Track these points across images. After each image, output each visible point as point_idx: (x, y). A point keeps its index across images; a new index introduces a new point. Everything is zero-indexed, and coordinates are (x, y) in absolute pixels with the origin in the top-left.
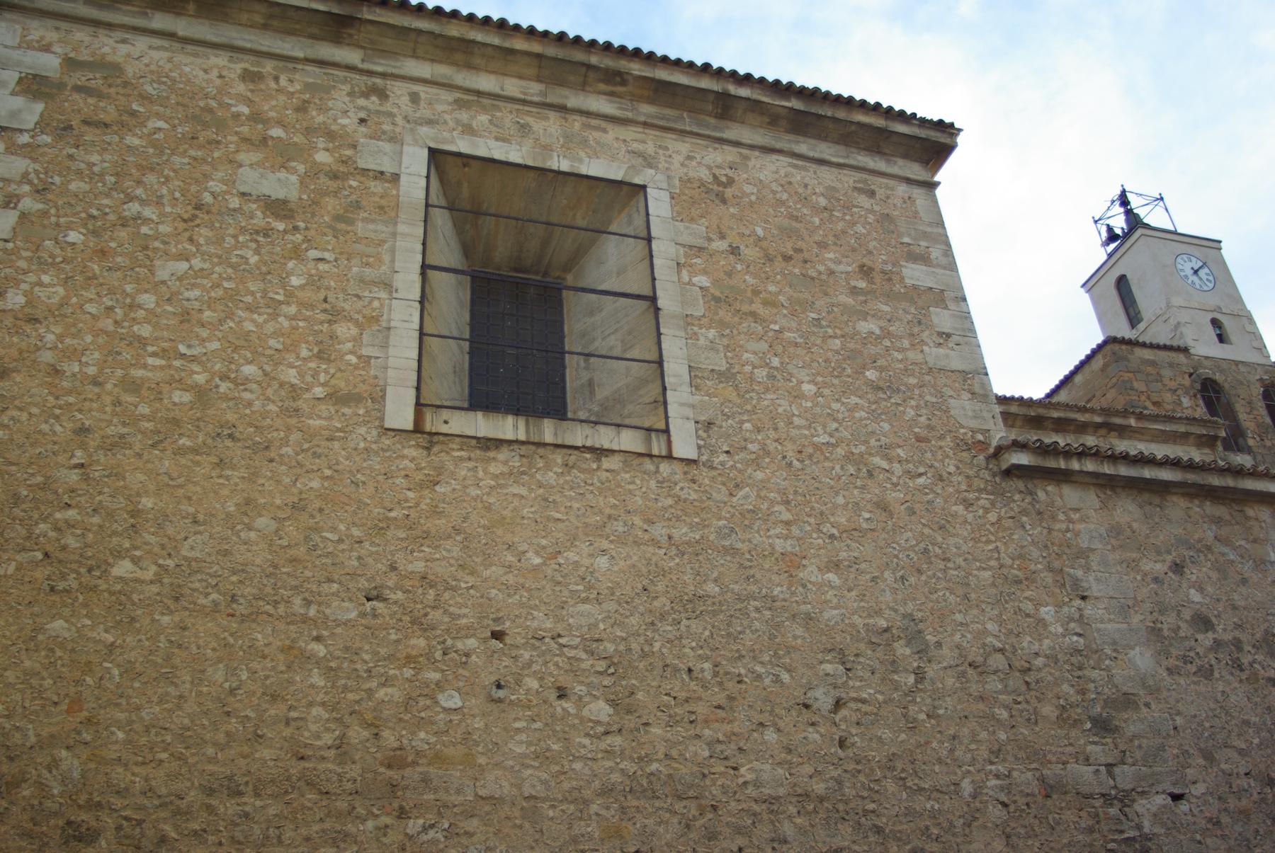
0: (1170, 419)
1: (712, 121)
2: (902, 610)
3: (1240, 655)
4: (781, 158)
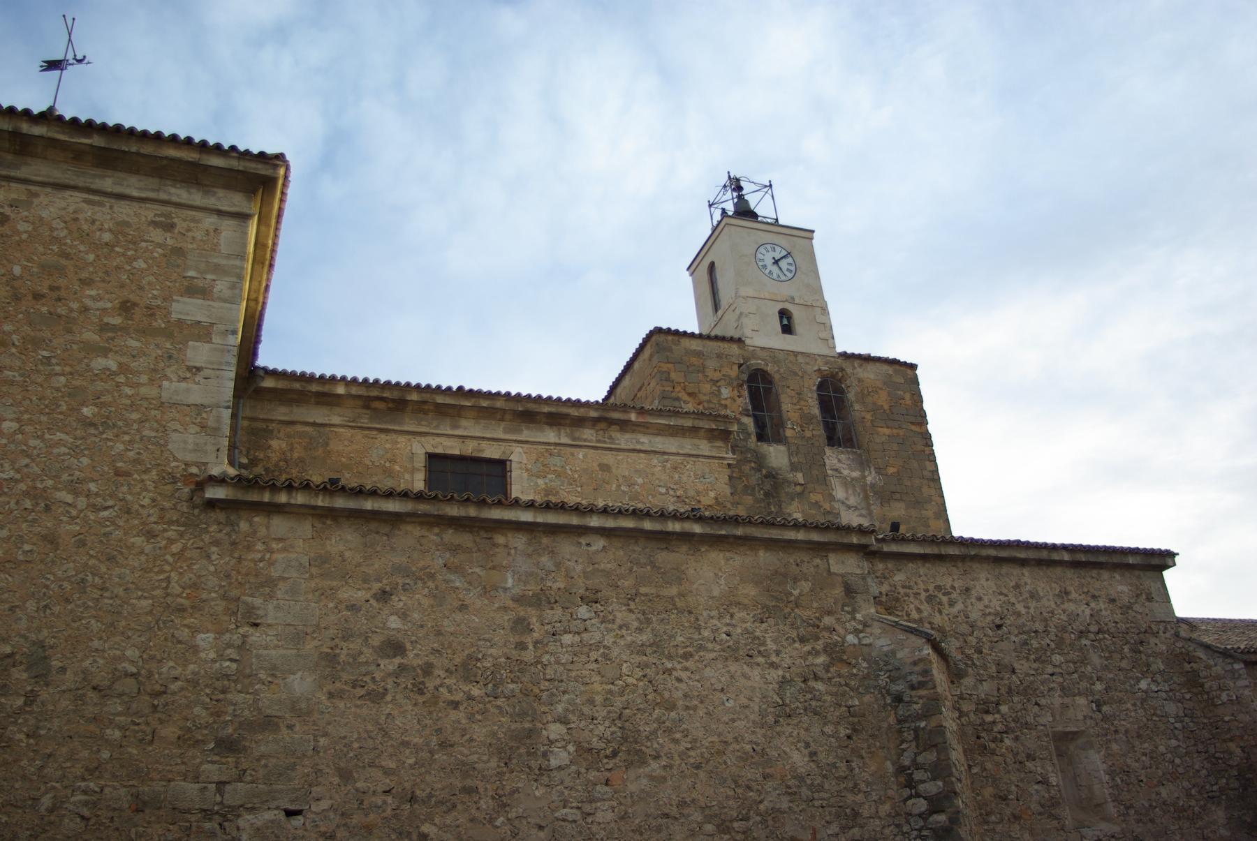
0: (676, 413)
1: (9, 157)
2: (33, 637)
3: (426, 680)
4: (76, 194)
